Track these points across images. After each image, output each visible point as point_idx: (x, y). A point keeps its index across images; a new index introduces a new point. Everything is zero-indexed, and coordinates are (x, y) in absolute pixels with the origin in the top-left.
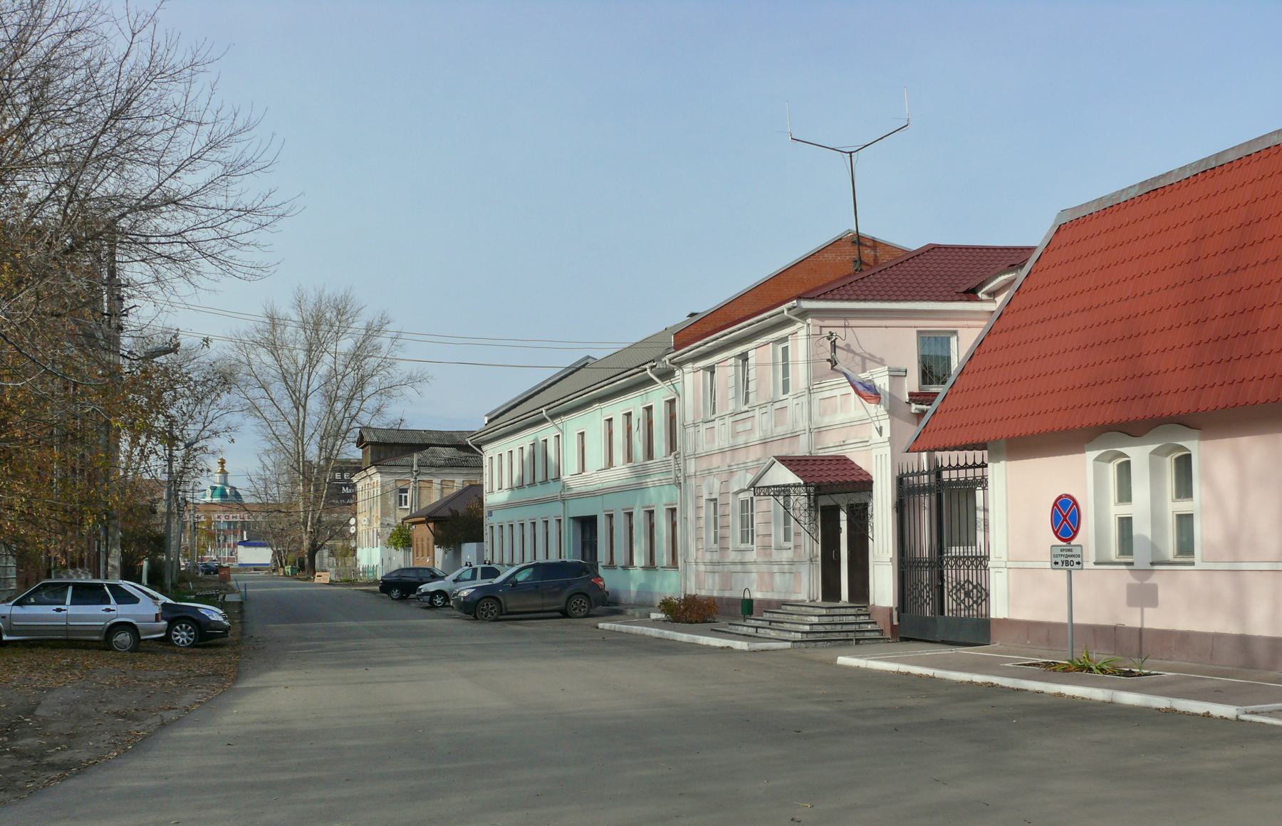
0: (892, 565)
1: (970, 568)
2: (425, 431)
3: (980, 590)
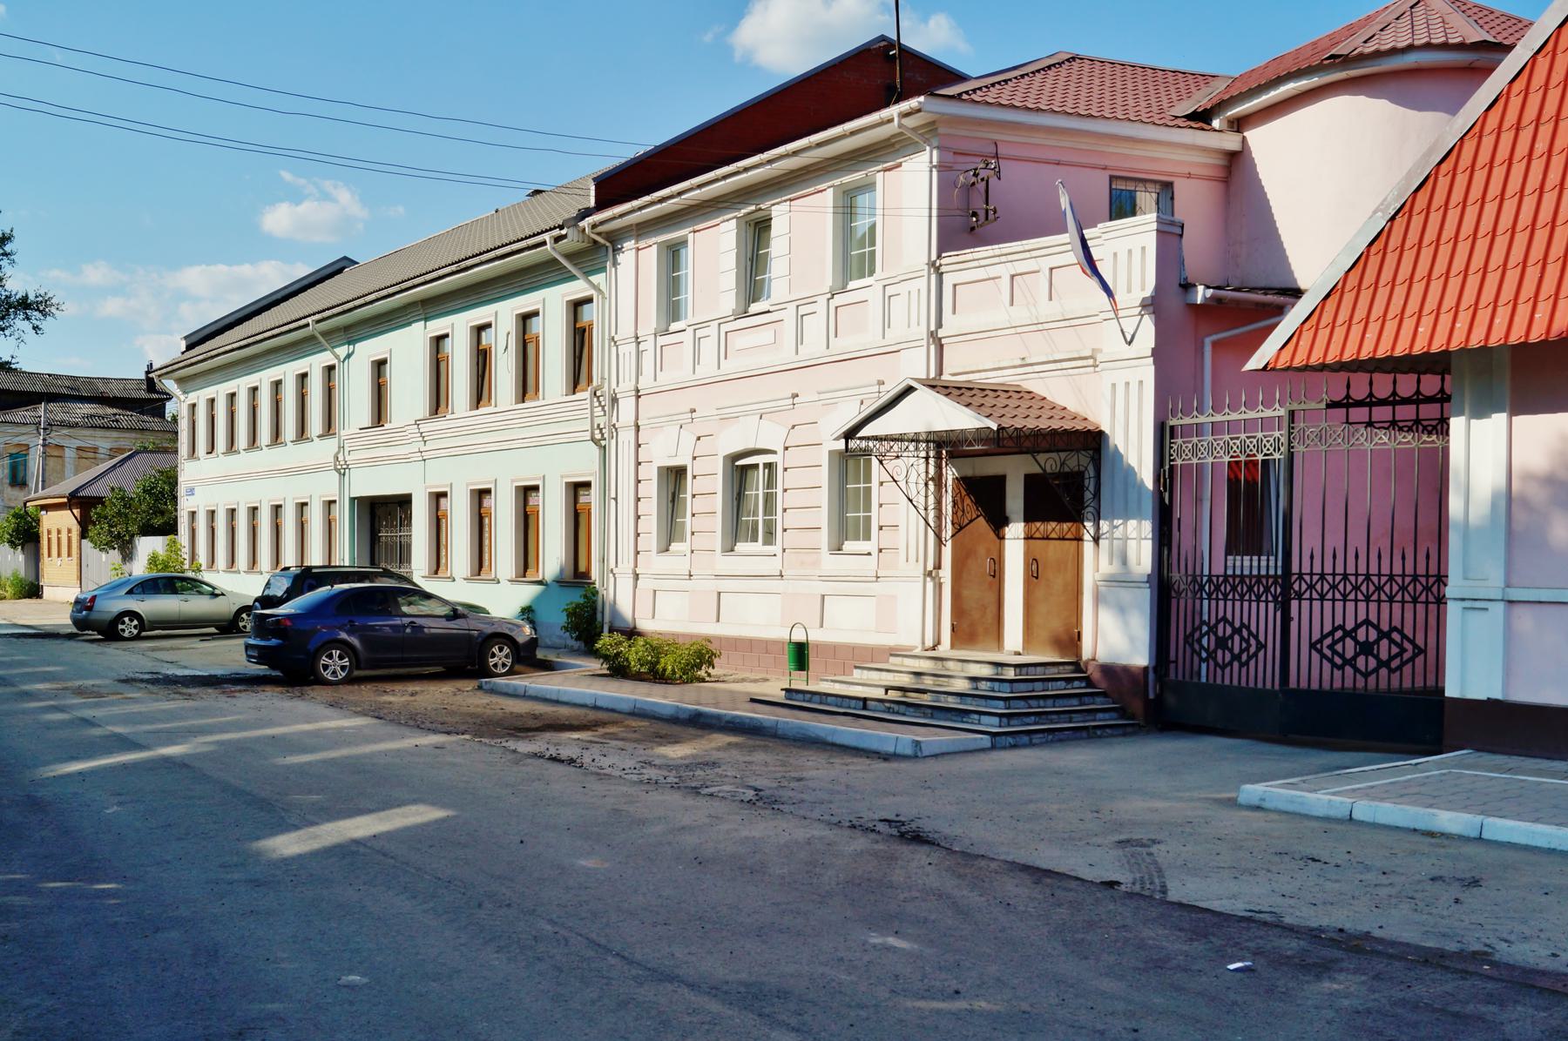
0: (1150, 587)
1: (1247, 597)
2: (50, 375)
3: (1246, 637)
